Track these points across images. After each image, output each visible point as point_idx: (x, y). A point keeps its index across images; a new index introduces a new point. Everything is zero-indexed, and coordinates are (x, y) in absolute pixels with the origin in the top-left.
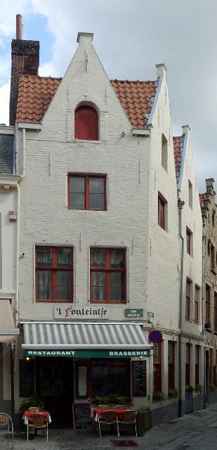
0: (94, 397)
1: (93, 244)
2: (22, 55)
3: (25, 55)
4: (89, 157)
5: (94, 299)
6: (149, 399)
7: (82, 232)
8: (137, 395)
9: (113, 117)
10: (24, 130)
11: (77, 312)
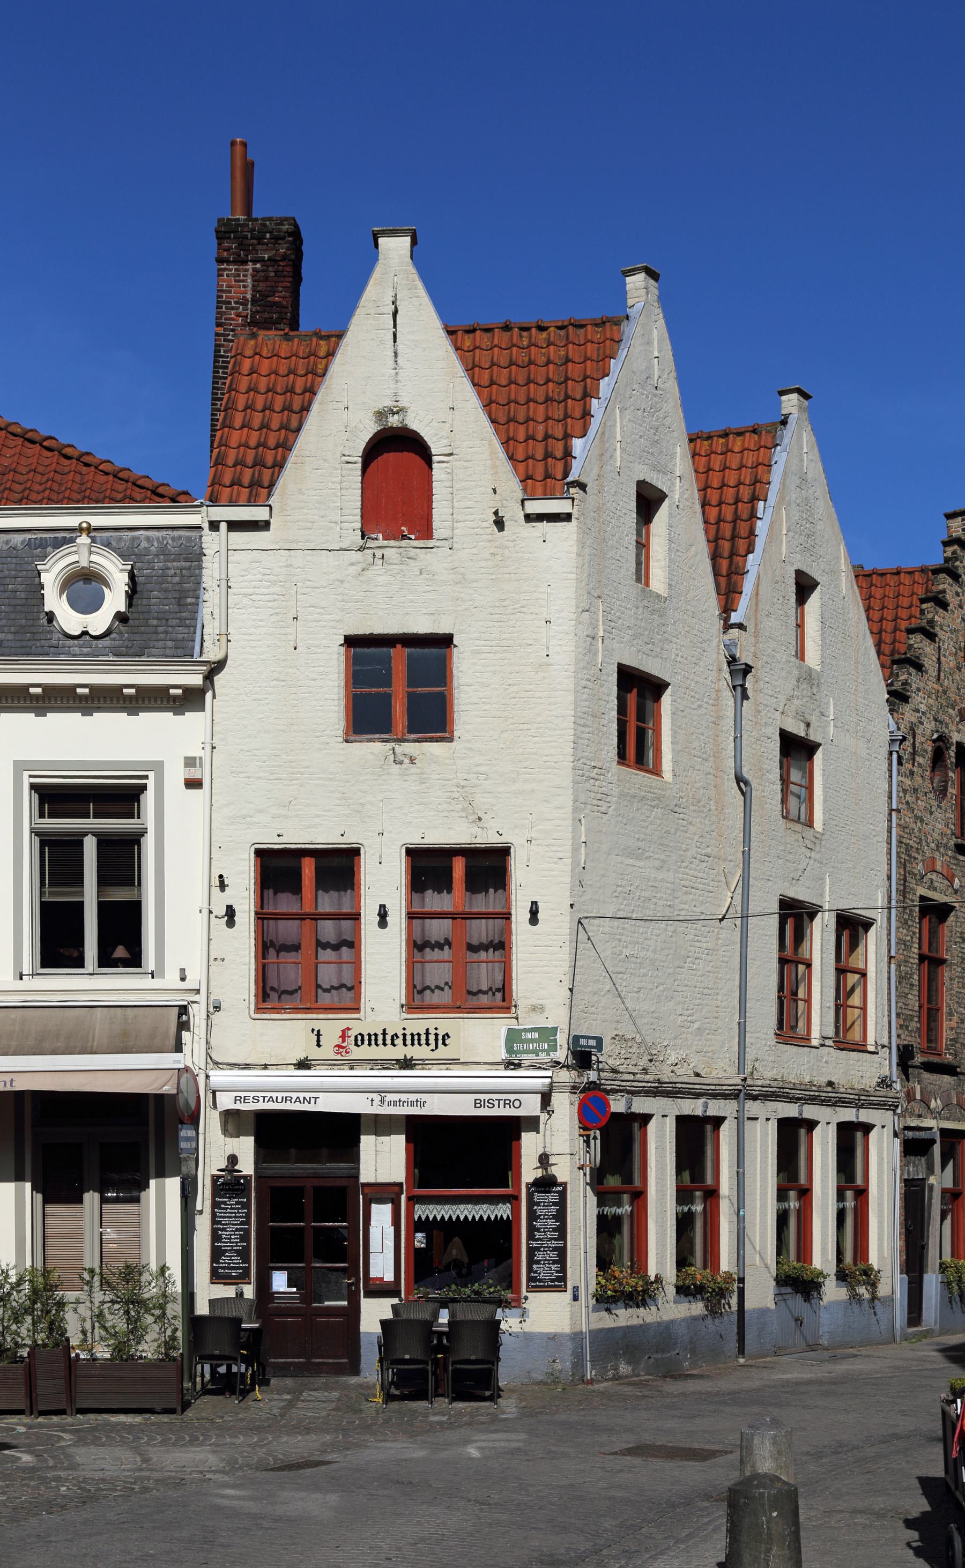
0: (163, 618)
1: (415, 839)
2: (245, 262)
3: (255, 261)
4: (400, 594)
5: (417, 998)
6: (576, 1298)
7: (386, 808)
8: (537, 1285)
9: (470, 461)
10: (223, 526)
11: (372, 1039)
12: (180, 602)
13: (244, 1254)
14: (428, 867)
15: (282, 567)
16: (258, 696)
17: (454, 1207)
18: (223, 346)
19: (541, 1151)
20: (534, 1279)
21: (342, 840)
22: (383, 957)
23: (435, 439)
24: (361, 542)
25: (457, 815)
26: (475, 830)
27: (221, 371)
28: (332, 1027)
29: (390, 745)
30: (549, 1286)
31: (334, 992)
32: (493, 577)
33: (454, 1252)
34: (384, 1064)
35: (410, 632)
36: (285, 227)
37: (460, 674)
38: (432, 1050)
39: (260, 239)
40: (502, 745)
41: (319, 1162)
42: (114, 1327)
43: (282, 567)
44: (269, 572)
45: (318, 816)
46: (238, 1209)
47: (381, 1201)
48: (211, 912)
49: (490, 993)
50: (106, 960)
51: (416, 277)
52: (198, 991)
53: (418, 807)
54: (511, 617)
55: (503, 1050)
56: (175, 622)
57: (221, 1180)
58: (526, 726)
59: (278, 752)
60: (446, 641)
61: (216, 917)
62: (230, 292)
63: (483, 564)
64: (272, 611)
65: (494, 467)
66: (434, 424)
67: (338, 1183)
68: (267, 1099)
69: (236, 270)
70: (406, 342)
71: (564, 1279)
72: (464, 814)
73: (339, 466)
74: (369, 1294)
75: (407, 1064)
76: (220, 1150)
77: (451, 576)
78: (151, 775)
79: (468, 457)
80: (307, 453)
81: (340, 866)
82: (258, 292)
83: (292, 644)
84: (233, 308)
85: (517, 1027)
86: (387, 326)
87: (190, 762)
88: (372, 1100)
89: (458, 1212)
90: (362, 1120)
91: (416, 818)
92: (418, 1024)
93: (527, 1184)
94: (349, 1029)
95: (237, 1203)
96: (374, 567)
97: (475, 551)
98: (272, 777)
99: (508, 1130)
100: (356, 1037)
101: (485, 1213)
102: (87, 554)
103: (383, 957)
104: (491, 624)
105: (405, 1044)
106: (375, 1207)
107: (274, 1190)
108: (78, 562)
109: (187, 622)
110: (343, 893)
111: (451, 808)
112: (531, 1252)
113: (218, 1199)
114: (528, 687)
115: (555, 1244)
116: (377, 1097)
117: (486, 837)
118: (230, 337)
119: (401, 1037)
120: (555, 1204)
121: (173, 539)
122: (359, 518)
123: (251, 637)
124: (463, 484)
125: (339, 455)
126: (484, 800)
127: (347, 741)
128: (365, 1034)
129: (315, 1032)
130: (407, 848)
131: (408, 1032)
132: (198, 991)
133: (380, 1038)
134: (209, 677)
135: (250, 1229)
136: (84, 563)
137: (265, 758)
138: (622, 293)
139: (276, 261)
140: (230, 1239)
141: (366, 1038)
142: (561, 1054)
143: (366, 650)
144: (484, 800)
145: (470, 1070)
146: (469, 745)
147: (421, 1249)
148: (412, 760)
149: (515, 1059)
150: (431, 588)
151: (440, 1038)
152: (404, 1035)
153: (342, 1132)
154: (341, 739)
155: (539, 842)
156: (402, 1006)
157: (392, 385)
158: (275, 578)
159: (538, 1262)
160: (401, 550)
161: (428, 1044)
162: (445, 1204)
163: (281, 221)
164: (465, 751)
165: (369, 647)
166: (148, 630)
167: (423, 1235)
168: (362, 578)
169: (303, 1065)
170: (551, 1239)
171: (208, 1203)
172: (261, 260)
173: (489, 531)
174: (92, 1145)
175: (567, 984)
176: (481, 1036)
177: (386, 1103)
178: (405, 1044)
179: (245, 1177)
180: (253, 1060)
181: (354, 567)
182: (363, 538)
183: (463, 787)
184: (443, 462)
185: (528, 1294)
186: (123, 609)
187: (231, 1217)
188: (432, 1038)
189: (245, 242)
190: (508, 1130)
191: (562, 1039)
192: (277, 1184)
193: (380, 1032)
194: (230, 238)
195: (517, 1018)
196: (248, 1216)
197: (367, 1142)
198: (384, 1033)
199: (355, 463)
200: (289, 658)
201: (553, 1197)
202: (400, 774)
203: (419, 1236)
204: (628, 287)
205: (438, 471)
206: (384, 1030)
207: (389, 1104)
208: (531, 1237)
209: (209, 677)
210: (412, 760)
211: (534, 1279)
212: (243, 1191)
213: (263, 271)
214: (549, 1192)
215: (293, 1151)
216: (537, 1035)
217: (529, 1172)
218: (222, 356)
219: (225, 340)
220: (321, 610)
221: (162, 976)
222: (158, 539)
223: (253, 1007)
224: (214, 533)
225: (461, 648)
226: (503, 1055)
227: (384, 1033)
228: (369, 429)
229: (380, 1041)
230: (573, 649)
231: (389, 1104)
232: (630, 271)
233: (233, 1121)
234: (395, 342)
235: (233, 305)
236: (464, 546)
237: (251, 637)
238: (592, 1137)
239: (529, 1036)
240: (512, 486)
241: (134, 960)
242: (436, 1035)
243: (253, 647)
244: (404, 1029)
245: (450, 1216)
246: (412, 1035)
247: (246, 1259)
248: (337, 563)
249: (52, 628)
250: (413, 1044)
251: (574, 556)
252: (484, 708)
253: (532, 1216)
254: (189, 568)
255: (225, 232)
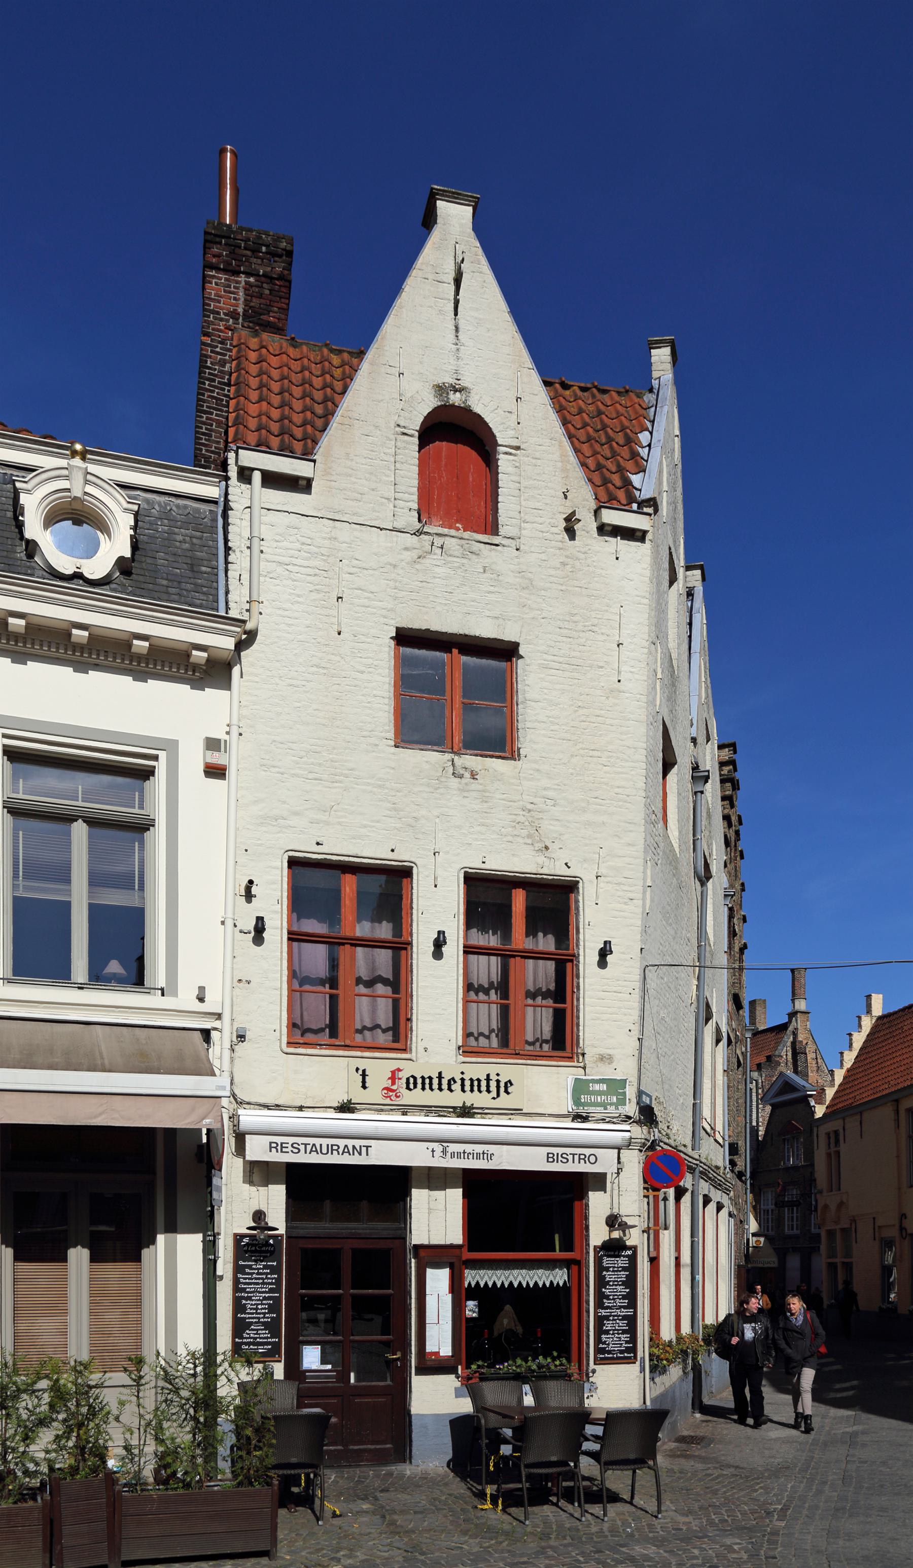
1: (475, 863)
2: (237, 273)
3: (249, 274)
4: (462, 591)
8: (605, 1357)
10: (257, 477)
11: (426, 1083)
12: (193, 567)
13: (273, 1327)
14: (487, 897)
15: (325, 538)
16: (295, 682)
17: (507, 1272)
18: (210, 357)
19: (608, 1213)
20: (603, 1351)
21: (391, 856)
22: (438, 991)
23: (501, 428)
24: (418, 526)
25: (521, 841)
26: (541, 859)
27: (207, 383)
28: (380, 1068)
29: (448, 756)
30: (618, 1358)
31: (367, 1033)
32: (563, 588)
33: (505, 1321)
34: (439, 1110)
35: (472, 634)
36: (283, 244)
37: (526, 688)
38: (494, 1098)
39: (255, 251)
40: (571, 771)
41: (357, 1220)
42: (173, 1439)
43: (325, 538)
44: (309, 541)
45: (365, 826)
46: (267, 1274)
47: (437, 1265)
48: (235, 926)
49: (538, 1044)
50: (98, 977)
51: (480, 251)
52: (219, 1016)
53: (479, 828)
54: (582, 634)
55: (570, 1102)
56: (189, 586)
57: (246, 1240)
58: (596, 753)
59: (319, 749)
60: (507, 652)
61: (241, 932)
62: (219, 302)
63: (552, 572)
64: (312, 587)
65: (564, 470)
66: (500, 411)
67: (382, 1245)
68: (309, 1148)
69: (226, 279)
70: (468, 318)
71: (634, 1350)
72: (530, 841)
73: (393, 437)
74: (421, 1371)
75: (466, 1112)
76: (244, 1203)
77: (518, 580)
78: (162, 755)
79: (537, 455)
80: (356, 416)
81: (389, 886)
82: (251, 307)
83: (336, 628)
84: (222, 320)
85: (584, 1078)
86: (446, 296)
87: (212, 744)
88: (433, 1151)
89: (511, 1278)
90: (414, 1174)
91: (476, 840)
92: (477, 1069)
93: (595, 1247)
94: (399, 1070)
95: (265, 1267)
96: (431, 556)
97: (543, 556)
98: (311, 776)
99: (577, 1186)
100: (408, 1079)
101: (540, 1278)
102: (82, 481)
103: (438, 991)
104: (560, 638)
105: (463, 1090)
106: (430, 1272)
107: (305, 1251)
108: (68, 490)
109: (205, 589)
110: (376, 924)
111: (516, 833)
112: (600, 1321)
113: (241, 1263)
114: (598, 712)
115: (624, 1312)
116: (438, 1147)
117: (551, 867)
118: (218, 350)
119: (459, 1082)
120: (624, 1269)
121: (178, 506)
122: (415, 498)
123: (286, 613)
124: (531, 482)
125: (392, 425)
126: (552, 827)
127: (396, 746)
128: (418, 1076)
129: (360, 1072)
130: (466, 873)
131: (467, 1077)
132: (219, 1016)
133: (435, 1082)
134: (241, 646)
135: (280, 1298)
136: (77, 492)
137: (303, 753)
138: (647, 365)
139: (272, 278)
140: (257, 1309)
141: (419, 1081)
142: (631, 1109)
143: (416, 652)
144: (552, 827)
145: (534, 1119)
146: (536, 766)
147: (472, 1319)
148: (473, 775)
149: (581, 1110)
150: (496, 589)
151: (502, 1085)
152: (463, 1080)
153: (390, 1187)
154: (393, 743)
155: (609, 879)
156: (459, 1048)
157: (452, 361)
158: (317, 550)
159: (607, 1332)
160: (463, 542)
161: (488, 1091)
162: (496, 1269)
163: (278, 239)
164: (532, 772)
165: (420, 648)
166: (157, 588)
167: (475, 1303)
168: (417, 566)
169: (346, 1108)
170: (621, 1307)
171: (230, 1268)
172: (256, 275)
173: (559, 537)
174: (108, 1187)
175: (636, 1034)
176: (544, 1085)
177: (449, 1155)
178: (463, 1090)
179: (275, 1237)
180: (284, 1099)
181: (409, 553)
182: (420, 520)
183: (530, 811)
184: (510, 454)
185: (596, 1367)
186: (128, 554)
187: (257, 1284)
188: (493, 1084)
189: (237, 251)
190: (577, 1186)
191: (631, 1092)
192: (310, 1245)
193: (435, 1075)
194: (220, 243)
195: (584, 1068)
196: (278, 1282)
197: (419, 1197)
198: (440, 1077)
199: (412, 436)
200: (332, 643)
201: (622, 1262)
202: (459, 790)
203: (471, 1304)
204: (653, 359)
205: (504, 462)
206: (440, 1073)
207: (453, 1155)
208: (599, 1305)
209: (241, 646)
210: (473, 775)
211: (603, 1351)
212: (272, 1253)
213: (257, 286)
214: (619, 1256)
215: (327, 1205)
216: (605, 1086)
217: (598, 1234)
218: (209, 368)
219: (211, 352)
220: (370, 595)
221: (175, 994)
222: (159, 504)
223: (285, 1040)
224: (243, 486)
225: (527, 660)
226: (568, 1106)
227: (440, 1077)
228: (428, 403)
229: (435, 1086)
230: (645, 678)
231: (453, 1155)
232: (657, 342)
233: (259, 1173)
234: (456, 314)
235: (222, 316)
236: (532, 550)
237: (286, 613)
238: (661, 1197)
239: (597, 1087)
240: (584, 498)
241: (137, 977)
242: (498, 1081)
243: (289, 625)
244: (462, 1073)
245: (486, 1283)
246: (472, 1080)
247: (275, 1333)
248: (389, 545)
249: (33, 564)
250: (472, 1091)
251: (647, 580)
252: (552, 728)
253: (601, 1282)
254: (201, 538)
255: (215, 235)
